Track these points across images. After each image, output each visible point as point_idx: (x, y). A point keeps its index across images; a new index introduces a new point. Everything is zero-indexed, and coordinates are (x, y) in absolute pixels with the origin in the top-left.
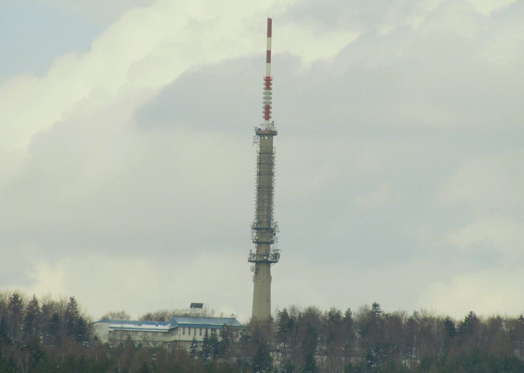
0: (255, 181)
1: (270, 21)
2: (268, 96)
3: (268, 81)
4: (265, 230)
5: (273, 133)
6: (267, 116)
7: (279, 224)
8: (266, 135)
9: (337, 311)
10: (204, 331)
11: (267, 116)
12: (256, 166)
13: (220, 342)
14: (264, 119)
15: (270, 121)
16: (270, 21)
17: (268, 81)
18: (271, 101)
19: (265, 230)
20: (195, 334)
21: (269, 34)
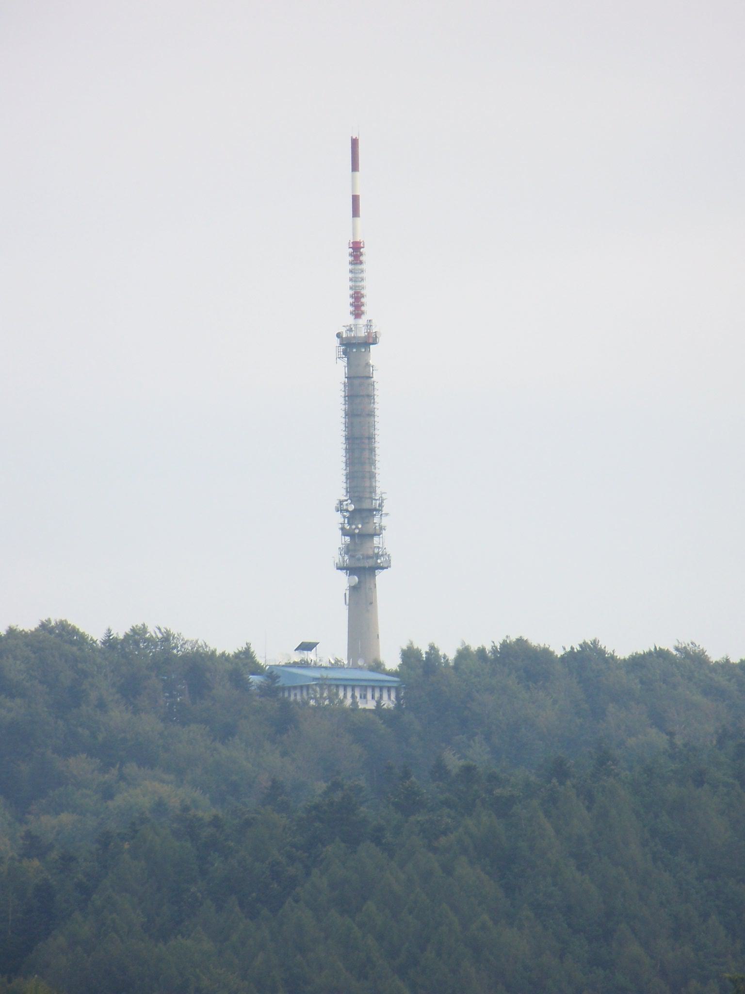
0: (343, 427)
1: (355, 143)
2: (358, 275)
3: (356, 249)
4: (361, 513)
5: (369, 341)
6: (357, 310)
7: (685, 640)
8: (355, 347)
9: (424, 649)
10: (377, 695)
11: (357, 310)
12: (342, 400)
13: (398, 706)
14: (353, 317)
15: (363, 321)
16: (355, 143)
17: (356, 249)
18: (350, 267)
19: (361, 513)
20: (381, 697)
21: (355, 167)
